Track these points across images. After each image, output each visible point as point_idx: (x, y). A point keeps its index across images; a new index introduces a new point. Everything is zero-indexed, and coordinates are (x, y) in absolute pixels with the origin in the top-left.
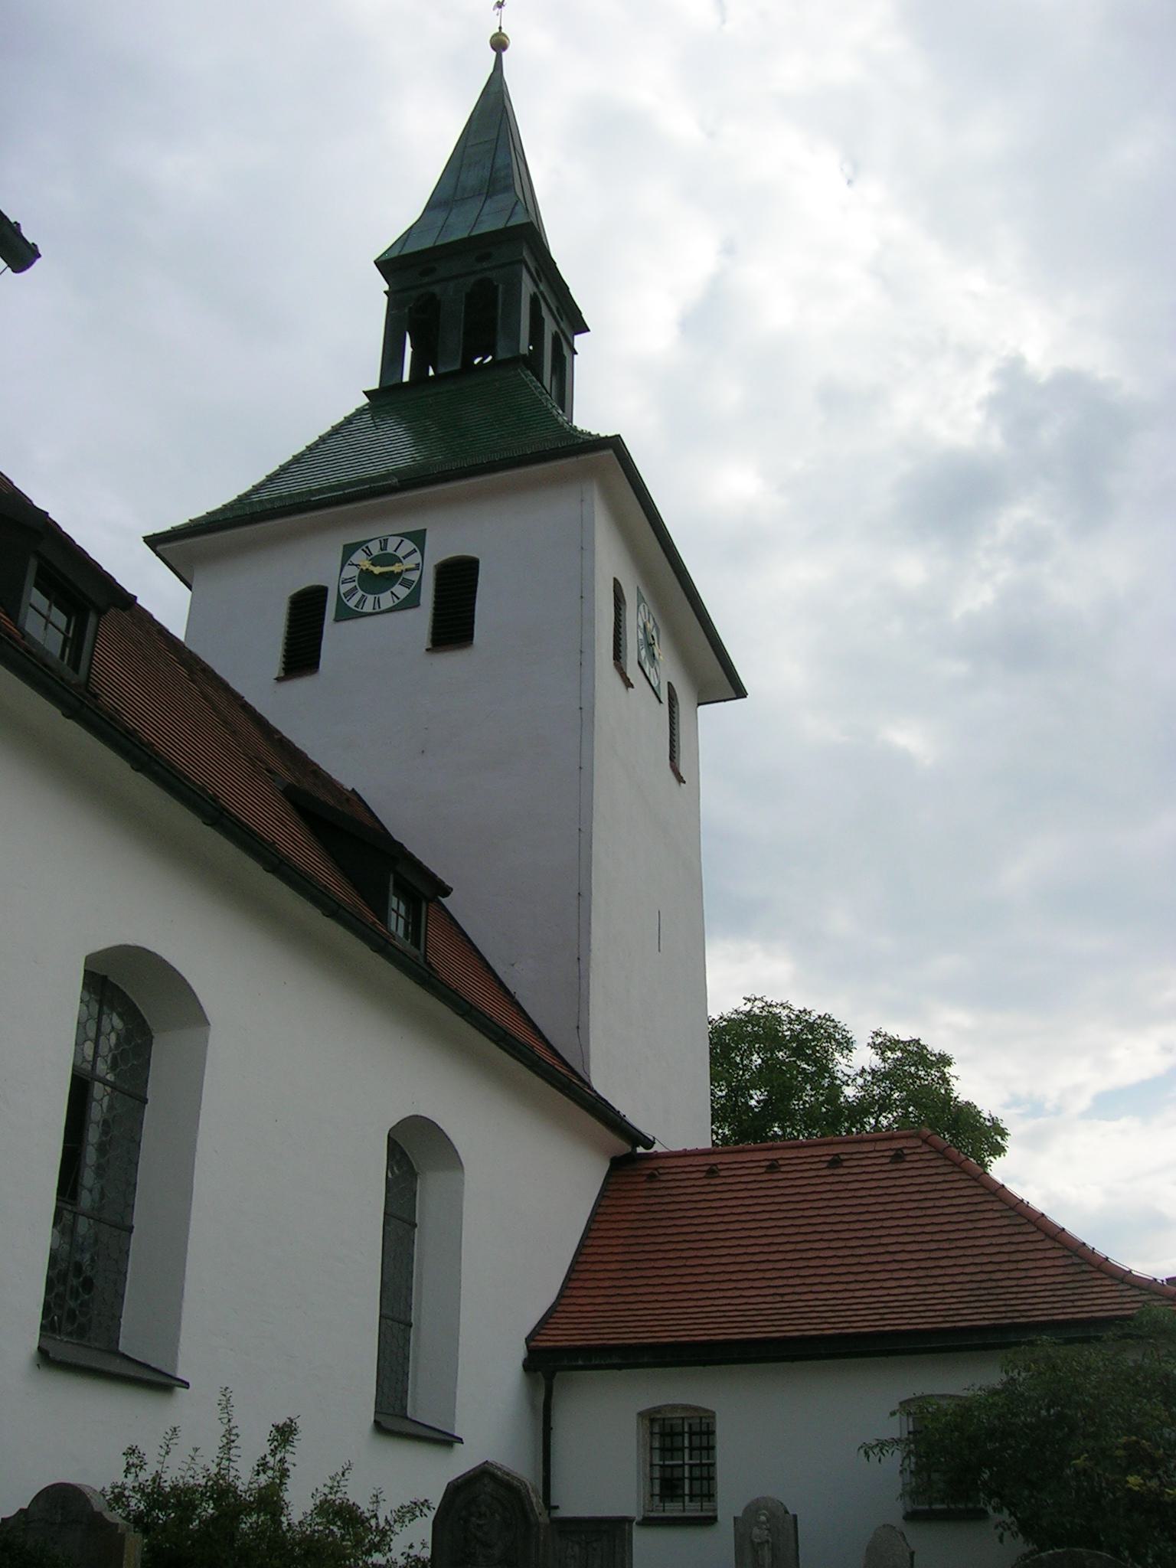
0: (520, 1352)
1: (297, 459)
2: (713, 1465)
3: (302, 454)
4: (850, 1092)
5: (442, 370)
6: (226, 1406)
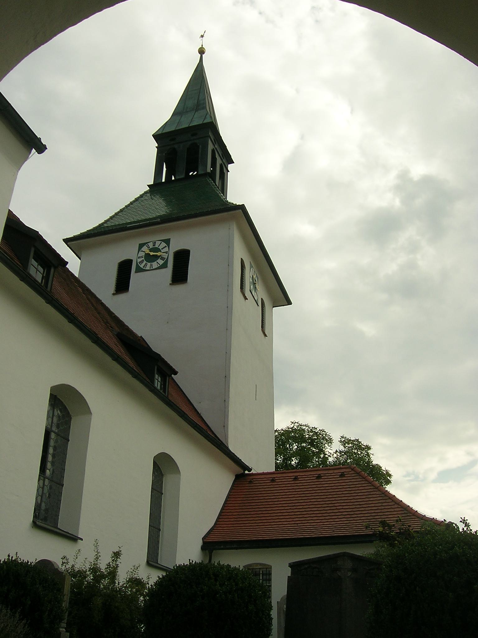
0: (200, 543)
1: (121, 211)
2: (271, 586)
3: (124, 209)
4: (331, 459)
5: (177, 178)
6: (96, 546)
